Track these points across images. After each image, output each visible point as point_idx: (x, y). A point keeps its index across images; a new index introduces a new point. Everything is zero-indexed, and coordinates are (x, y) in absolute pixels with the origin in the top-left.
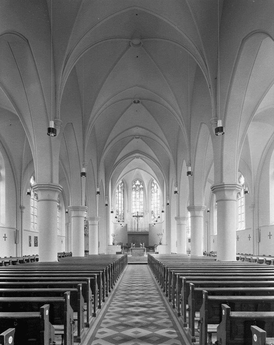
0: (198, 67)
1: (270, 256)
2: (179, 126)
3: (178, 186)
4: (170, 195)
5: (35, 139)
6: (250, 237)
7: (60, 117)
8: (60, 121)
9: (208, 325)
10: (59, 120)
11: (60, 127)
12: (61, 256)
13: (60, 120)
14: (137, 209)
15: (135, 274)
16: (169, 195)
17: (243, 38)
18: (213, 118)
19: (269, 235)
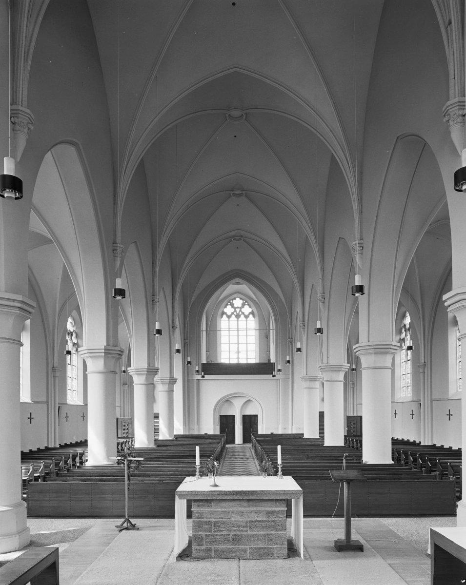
0: (333, 160)
1: (357, 413)
2: (307, 237)
3: (327, 300)
4: (294, 338)
5: (83, 271)
6: (67, 417)
7: (25, 103)
8: (27, 113)
9: (260, 432)
10: (20, 108)
11: (26, 130)
12: (30, 450)
13: (28, 111)
14: (246, 331)
15: (242, 472)
16: (292, 338)
17: (239, 392)
18: (457, 100)
19: (32, 419)
